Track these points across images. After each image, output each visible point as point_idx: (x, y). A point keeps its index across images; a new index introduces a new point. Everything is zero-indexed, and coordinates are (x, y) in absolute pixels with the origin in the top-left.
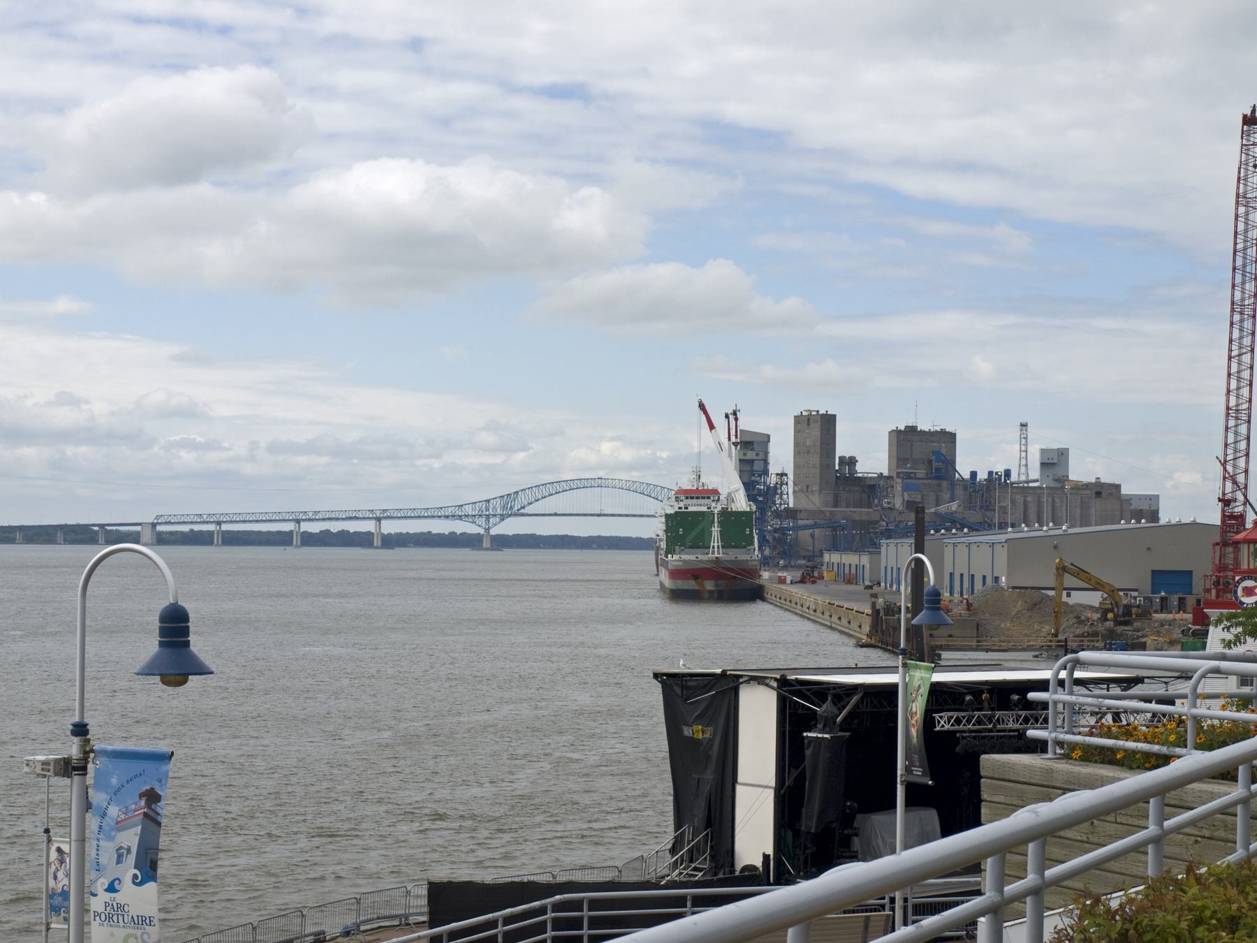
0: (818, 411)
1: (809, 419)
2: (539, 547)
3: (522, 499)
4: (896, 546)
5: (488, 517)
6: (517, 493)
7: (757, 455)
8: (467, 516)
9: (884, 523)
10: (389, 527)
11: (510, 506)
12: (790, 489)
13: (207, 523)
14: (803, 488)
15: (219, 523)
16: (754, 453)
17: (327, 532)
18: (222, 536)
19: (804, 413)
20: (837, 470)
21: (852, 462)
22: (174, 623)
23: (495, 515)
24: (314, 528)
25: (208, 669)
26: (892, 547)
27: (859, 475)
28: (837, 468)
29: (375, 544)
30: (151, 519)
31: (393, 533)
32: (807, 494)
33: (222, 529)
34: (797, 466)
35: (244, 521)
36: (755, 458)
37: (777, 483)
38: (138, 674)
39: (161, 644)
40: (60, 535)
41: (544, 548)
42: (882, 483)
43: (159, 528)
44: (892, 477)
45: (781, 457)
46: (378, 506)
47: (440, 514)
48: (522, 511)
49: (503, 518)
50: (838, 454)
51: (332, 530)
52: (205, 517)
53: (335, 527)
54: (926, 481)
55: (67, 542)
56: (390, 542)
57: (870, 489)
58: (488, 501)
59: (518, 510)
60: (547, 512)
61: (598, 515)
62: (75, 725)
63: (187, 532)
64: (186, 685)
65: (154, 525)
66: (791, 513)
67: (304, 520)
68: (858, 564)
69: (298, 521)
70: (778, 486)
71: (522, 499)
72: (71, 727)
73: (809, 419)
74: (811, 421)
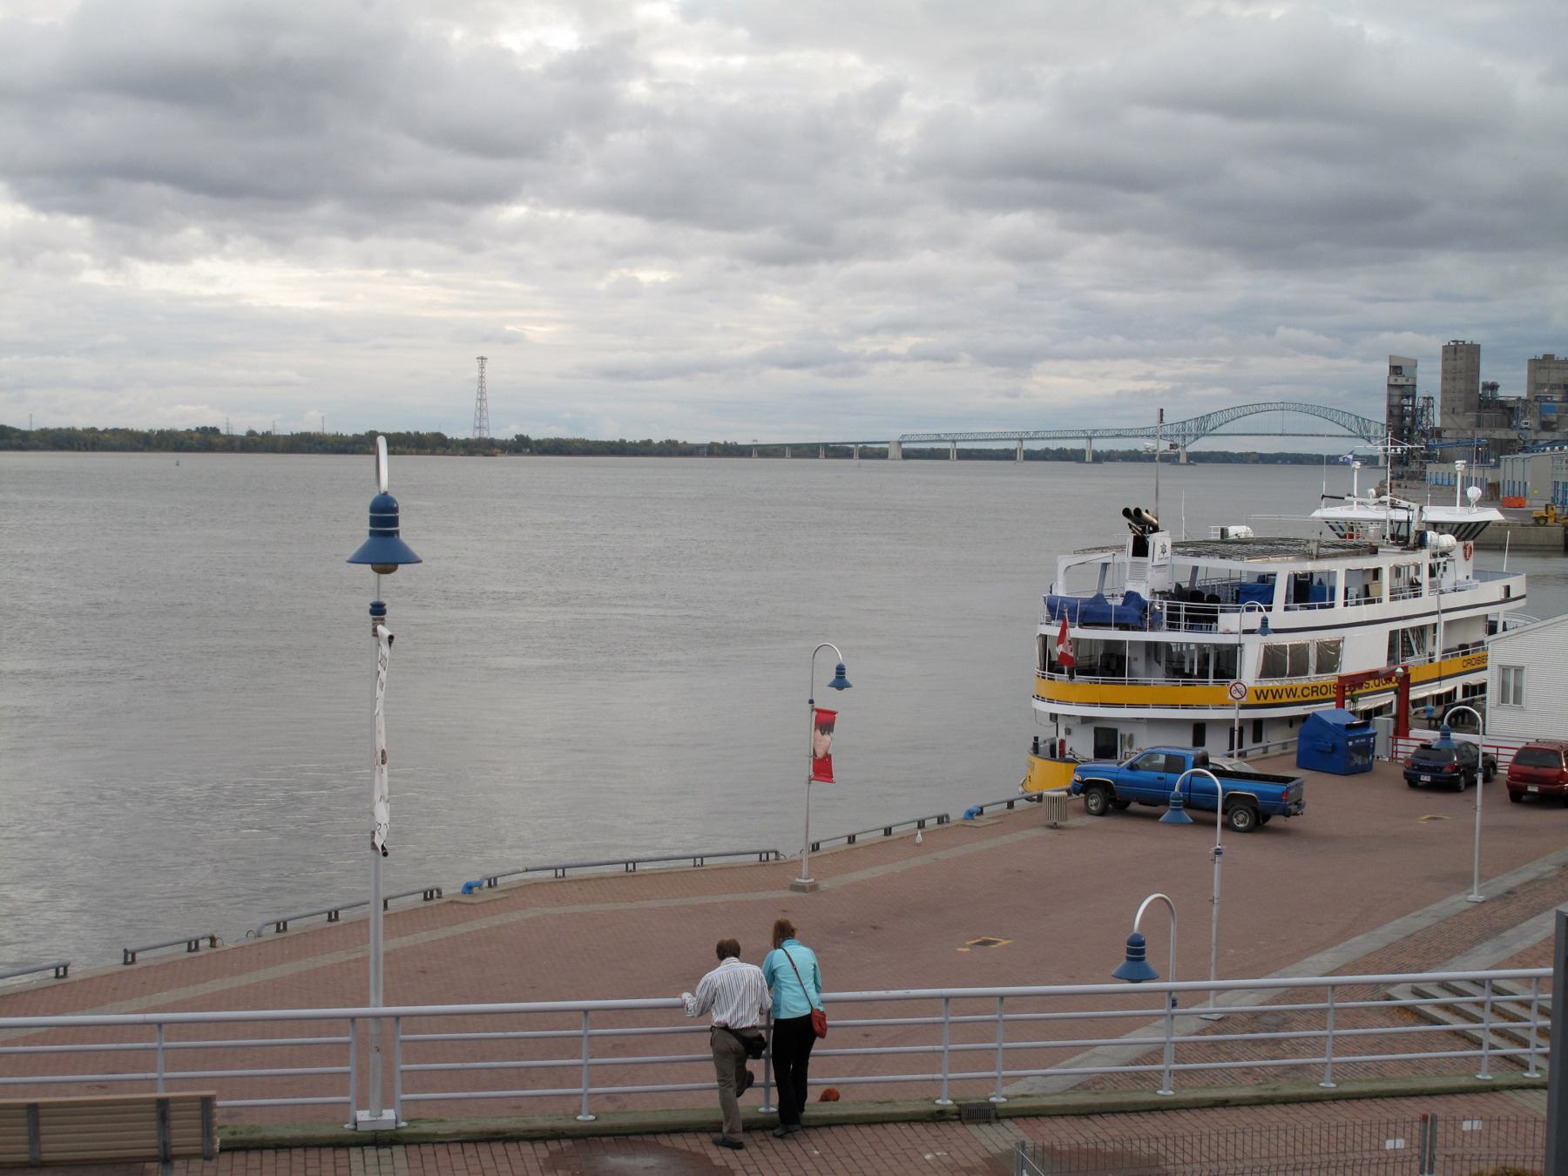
0: (1464, 342)
1: (1456, 349)
2: (1231, 462)
3: (1214, 421)
4: (1512, 461)
5: (1184, 436)
6: (1210, 415)
7: (1407, 380)
8: (1166, 436)
9: (1522, 442)
10: (1102, 445)
11: (1203, 426)
12: (1437, 410)
13: (944, 441)
14: (1449, 411)
15: (954, 441)
16: (1404, 379)
17: (1047, 451)
18: (957, 453)
19: (1452, 344)
20: (1480, 395)
21: (1494, 387)
22: (378, 513)
23: (1190, 435)
24: (1037, 446)
25: (415, 556)
26: (1509, 462)
27: (1500, 399)
28: (1480, 392)
29: (1087, 460)
30: (897, 438)
31: (412, 432)
32: (1453, 416)
33: (957, 447)
34: (1444, 391)
35: (920, 441)
36: (1405, 383)
37: (1423, 406)
38: (351, 562)
39: (372, 533)
40: (822, 452)
41: (1235, 463)
42: (1520, 405)
43: (904, 446)
44: (1530, 401)
45: (1429, 381)
46: (1090, 425)
47: (1142, 434)
48: (1214, 432)
49: (1197, 437)
50: (1482, 380)
51: (1051, 448)
52: (942, 436)
53: (1054, 445)
54: (1561, 404)
55: (793, 456)
56: (1099, 458)
57: (1508, 412)
58: (1184, 423)
59: (1210, 430)
60: (1236, 432)
61: (1280, 435)
62: (373, 605)
63: (79, 431)
64: (393, 574)
65: (900, 443)
66: (1438, 433)
67: (1027, 439)
68: (1521, 480)
69: (1021, 440)
70: (1425, 408)
71: (1214, 421)
72: (370, 607)
73: (1456, 349)
74: (1458, 350)
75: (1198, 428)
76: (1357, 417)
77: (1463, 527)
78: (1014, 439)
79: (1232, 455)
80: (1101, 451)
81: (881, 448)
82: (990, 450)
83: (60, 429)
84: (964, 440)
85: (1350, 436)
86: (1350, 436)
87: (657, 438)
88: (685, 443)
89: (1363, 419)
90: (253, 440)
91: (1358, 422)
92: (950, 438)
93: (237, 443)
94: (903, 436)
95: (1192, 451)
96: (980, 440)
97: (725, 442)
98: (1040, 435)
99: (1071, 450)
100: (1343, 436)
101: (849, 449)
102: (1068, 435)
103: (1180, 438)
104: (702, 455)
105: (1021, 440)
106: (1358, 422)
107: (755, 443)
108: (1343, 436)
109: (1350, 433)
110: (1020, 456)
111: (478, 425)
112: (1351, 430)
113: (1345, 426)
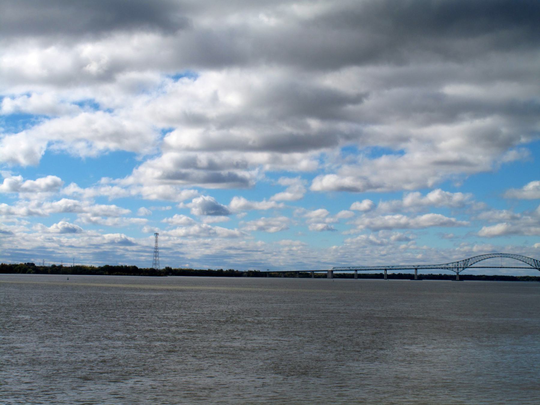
3: (471, 261)
8: (450, 268)
11: (466, 263)
15: (356, 270)
23: (461, 268)
29: (415, 279)
31: (124, 266)
43: (334, 272)
47: (440, 267)
48: (471, 266)
49: (464, 268)
52: (351, 268)
53: (396, 272)
58: (458, 262)
65: (332, 271)
67: (388, 269)
71: (471, 261)
75: (464, 265)
76: (534, 260)
77: (52, 240)
78: (383, 269)
79: (474, 276)
80: (5, 264)
81: (344, 274)
82: (368, 274)
83: (429, 275)
84: (361, 270)
85: (531, 268)
86: (531, 268)
87: (225, 269)
88: (237, 271)
89: (537, 261)
90: (56, 269)
91: (535, 262)
92: (355, 269)
93: (49, 271)
94: (334, 268)
95: (461, 274)
96: (434, 268)
97: (255, 270)
98: (430, 267)
99: (404, 274)
100: (528, 268)
101: (308, 274)
102: (438, 267)
103: (456, 269)
104: (245, 276)
105: (386, 270)
106: (535, 262)
107: (268, 271)
108: (528, 268)
109: (530, 266)
110: (458, 278)
111: (154, 263)
112: (531, 265)
113: (529, 264)
